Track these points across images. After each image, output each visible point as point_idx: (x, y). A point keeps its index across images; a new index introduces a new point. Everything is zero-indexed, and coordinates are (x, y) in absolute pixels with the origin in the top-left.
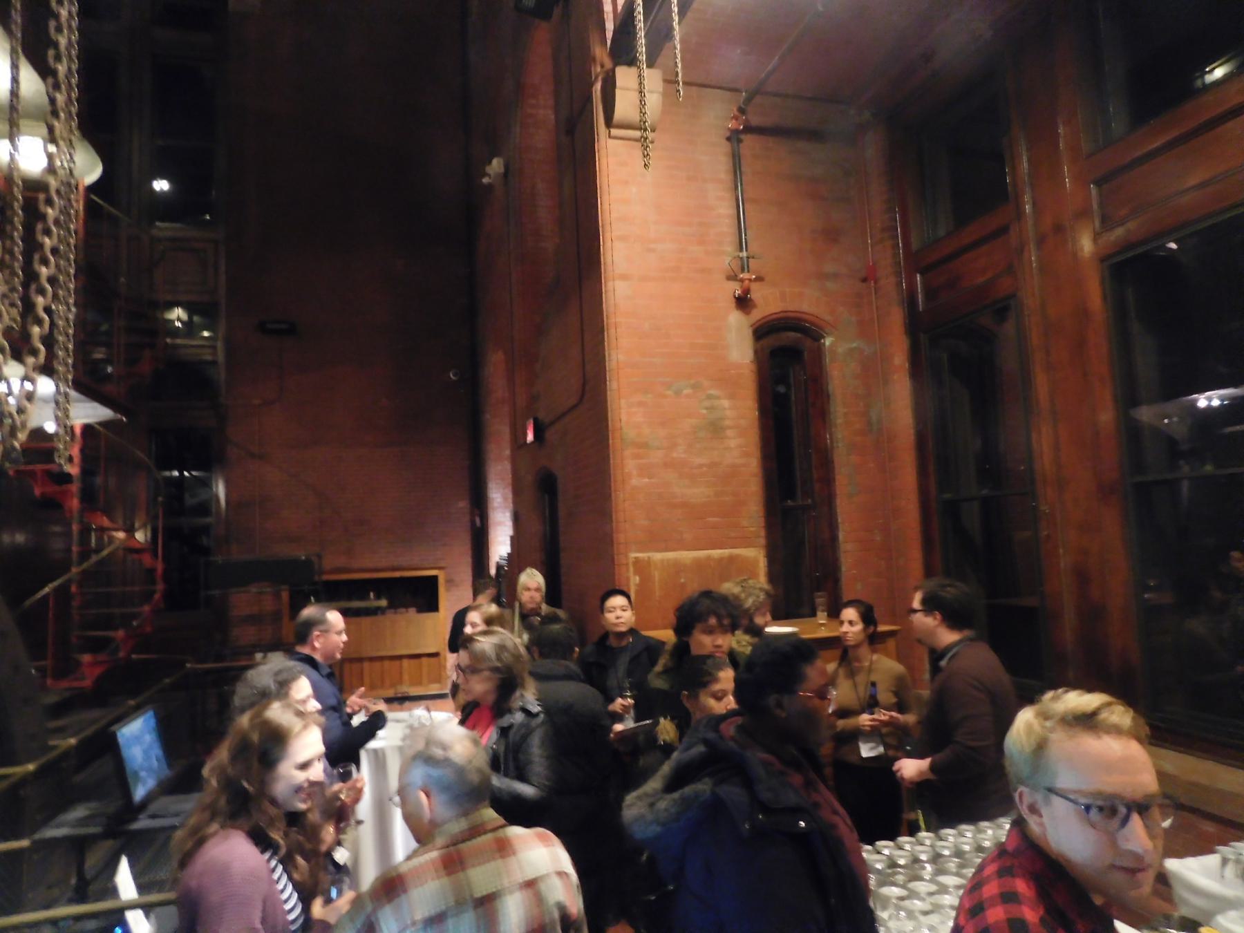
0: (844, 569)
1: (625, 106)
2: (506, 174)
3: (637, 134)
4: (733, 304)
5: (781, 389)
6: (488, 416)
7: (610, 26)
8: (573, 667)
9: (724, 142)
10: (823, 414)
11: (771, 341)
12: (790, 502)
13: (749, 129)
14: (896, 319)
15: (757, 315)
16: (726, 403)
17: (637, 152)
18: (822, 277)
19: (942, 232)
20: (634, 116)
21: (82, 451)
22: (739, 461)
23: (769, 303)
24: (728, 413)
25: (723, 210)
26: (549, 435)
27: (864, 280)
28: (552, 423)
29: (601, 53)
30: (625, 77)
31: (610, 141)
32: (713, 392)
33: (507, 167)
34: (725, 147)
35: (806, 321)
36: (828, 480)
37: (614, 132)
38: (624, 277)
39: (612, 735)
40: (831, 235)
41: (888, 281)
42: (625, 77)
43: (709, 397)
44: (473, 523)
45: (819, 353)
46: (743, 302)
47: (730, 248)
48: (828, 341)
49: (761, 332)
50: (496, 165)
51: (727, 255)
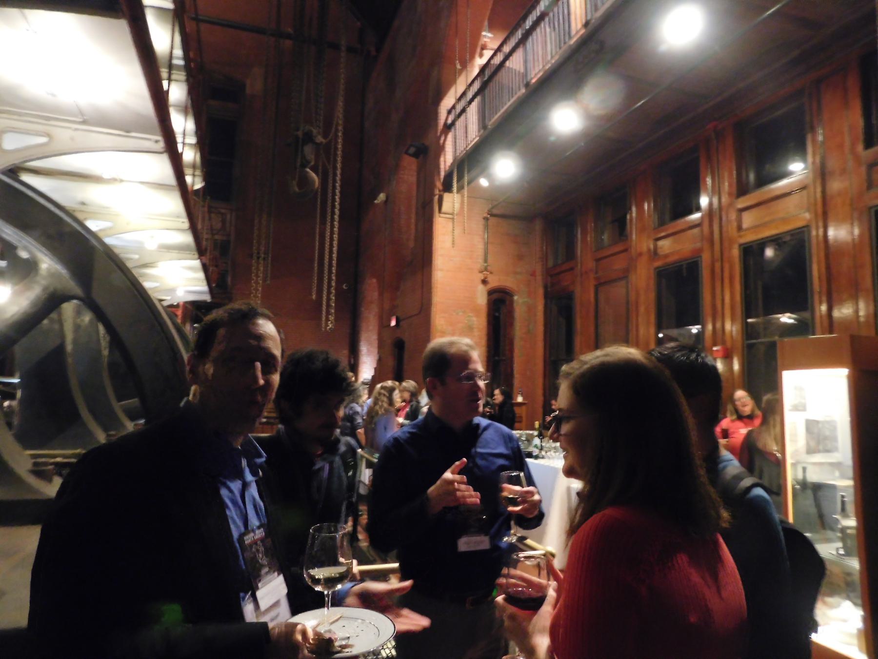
0: (515, 384)
1: (446, 207)
2: (386, 202)
3: (450, 216)
4: (480, 282)
5: (497, 314)
6: (363, 309)
7: (442, 174)
8: (589, 18)
9: (482, 220)
10: (511, 324)
11: (495, 296)
12: (497, 358)
13: (492, 215)
14: (541, 291)
15: (490, 286)
16: (474, 319)
17: (450, 224)
18: (516, 273)
19: (560, 262)
20: (450, 211)
21: (183, 312)
22: (791, 476)
23: (495, 282)
24: (475, 323)
25: (480, 247)
26: (401, 323)
27: (532, 275)
28: (404, 319)
29: (439, 185)
30: (447, 197)
31: (440, 218)
32: (470, 314)
33: (387, 198)
34: (482, 222)
35: (507, 289)
36: (511, 351)
37: (442, 215)
38: (442, 270)
39: (484, 182)
40: (520, 257)
41: (539, 278)
42: (447, 197)
43: (469, 316)
44: (350, 361)
45: (512, 302)
46: (484, 282)
47: (481, 260)
48: (516, 298)
49: (490, 293)
50: (382, 197)
51: (479, 263)
